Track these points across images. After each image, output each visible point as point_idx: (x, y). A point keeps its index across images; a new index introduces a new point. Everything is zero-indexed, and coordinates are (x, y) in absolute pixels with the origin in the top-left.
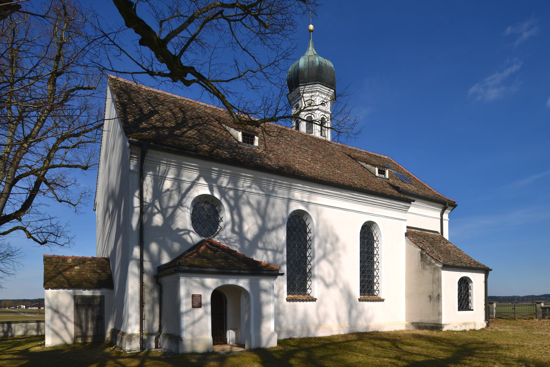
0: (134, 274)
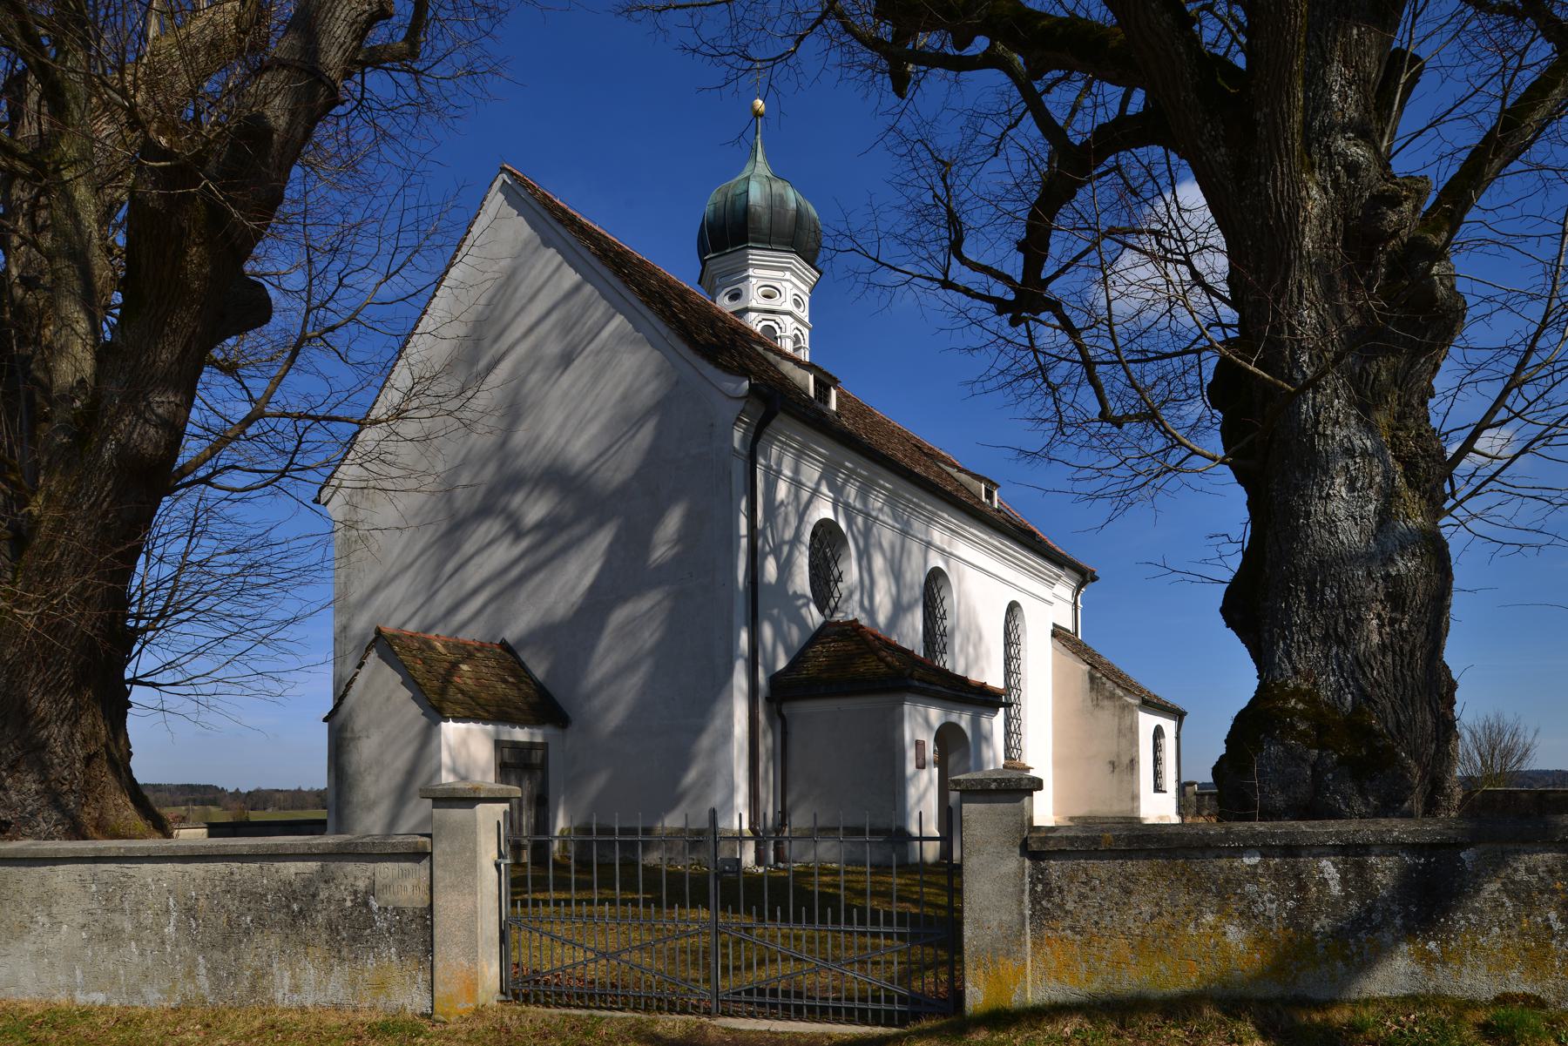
0: (740, 689)
